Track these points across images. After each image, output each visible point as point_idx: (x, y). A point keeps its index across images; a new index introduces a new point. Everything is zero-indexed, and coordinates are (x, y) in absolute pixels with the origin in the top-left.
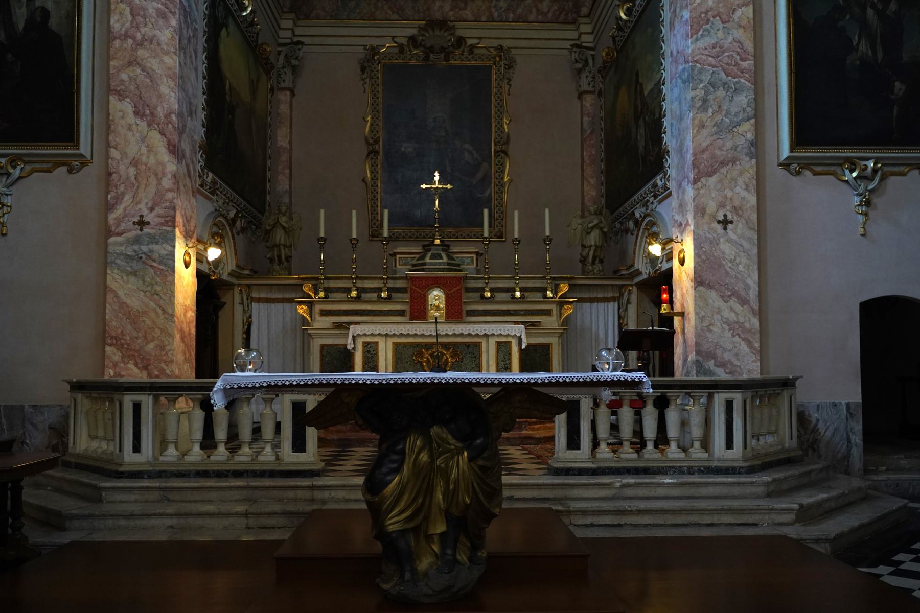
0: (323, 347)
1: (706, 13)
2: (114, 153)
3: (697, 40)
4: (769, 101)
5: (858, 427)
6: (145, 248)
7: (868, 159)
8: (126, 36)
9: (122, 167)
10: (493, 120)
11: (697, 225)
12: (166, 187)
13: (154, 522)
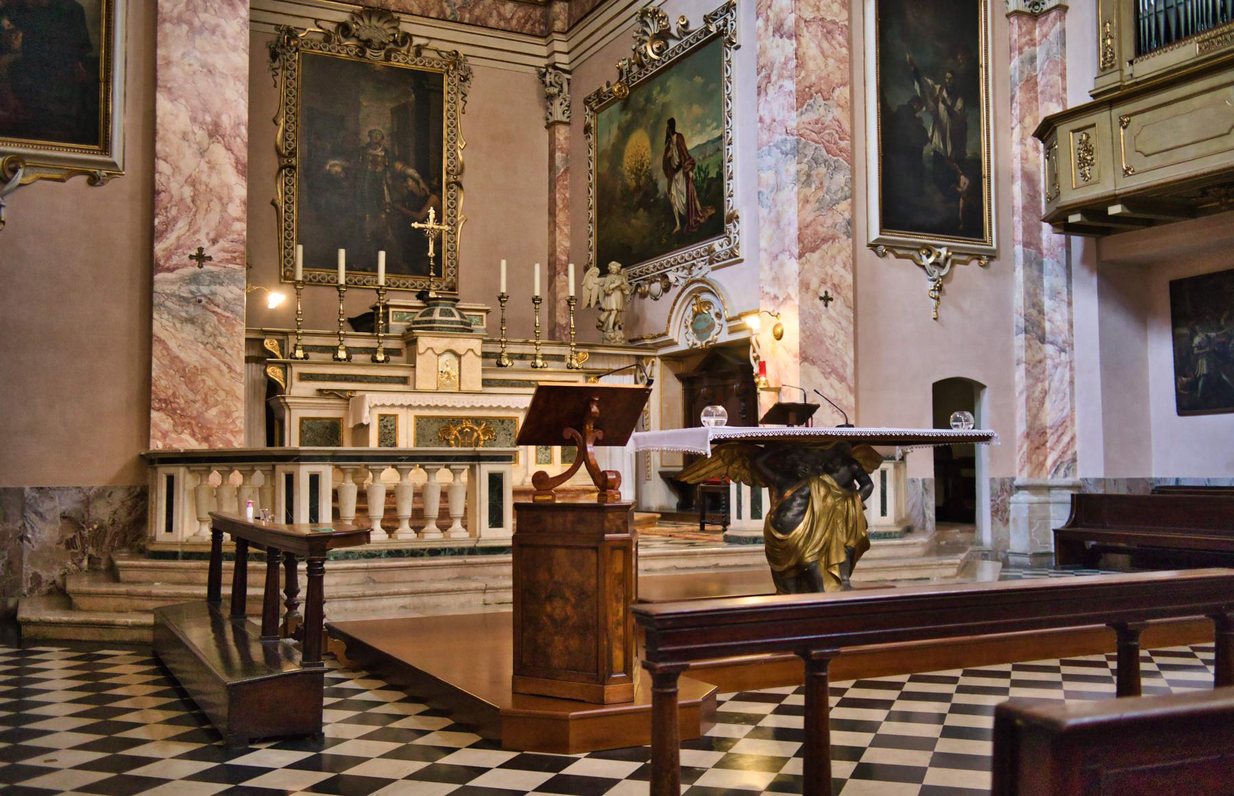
0: (302, 420)
1: (810, 87)
2: (161, 165)
3: (802, 114)
4: (860, 179)
5: (931, 502)
6: (205, 290)
7: (941, 247)
8: (180, 20)
9: (174, 187)
10: (445, 143)
11: (801, 300)
12: (234, 215)
13: (385, 602)
